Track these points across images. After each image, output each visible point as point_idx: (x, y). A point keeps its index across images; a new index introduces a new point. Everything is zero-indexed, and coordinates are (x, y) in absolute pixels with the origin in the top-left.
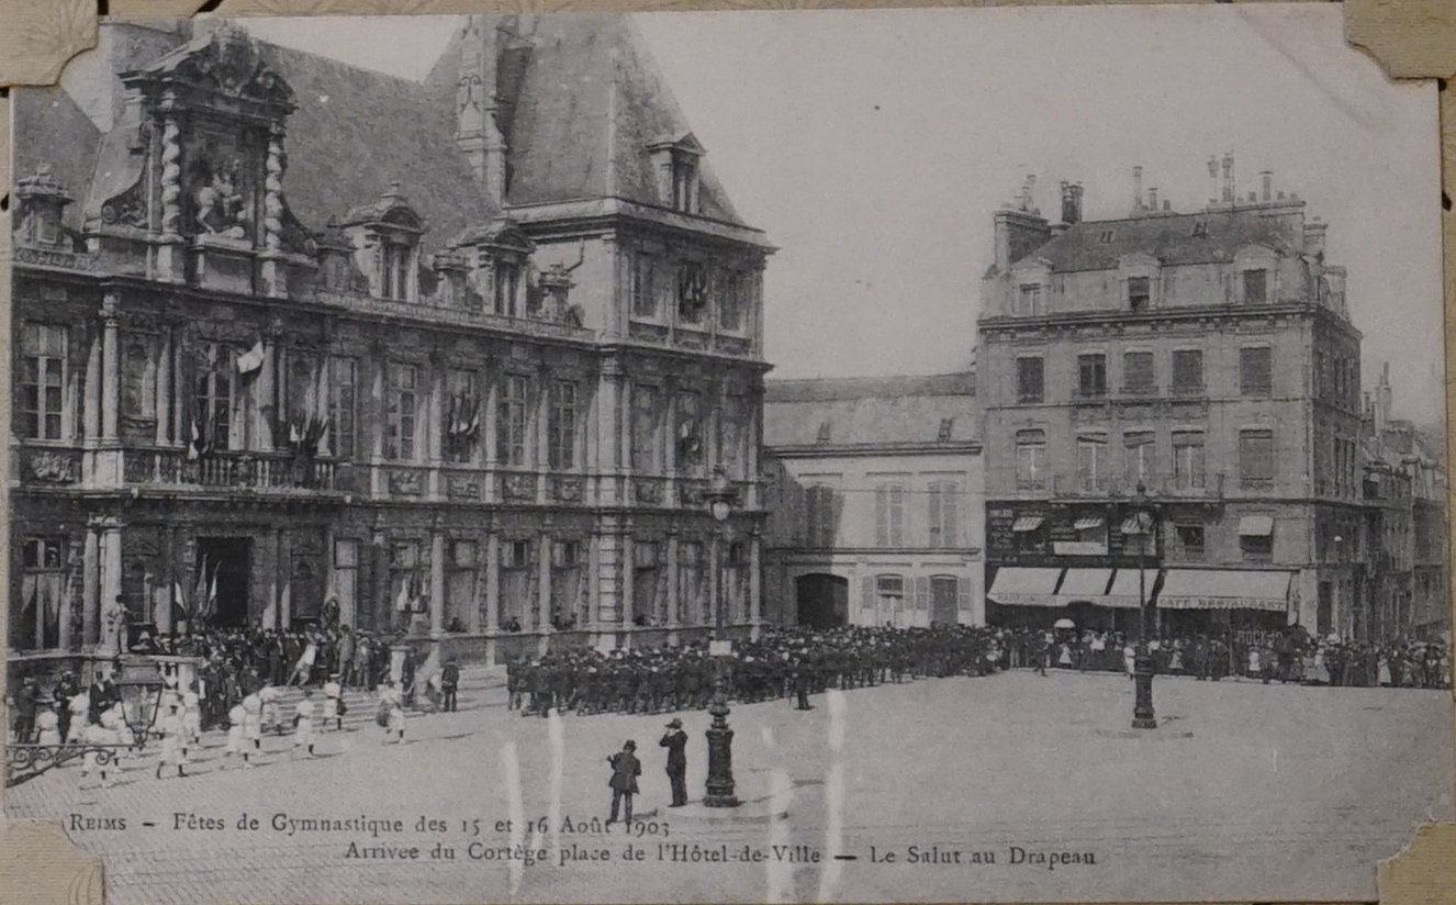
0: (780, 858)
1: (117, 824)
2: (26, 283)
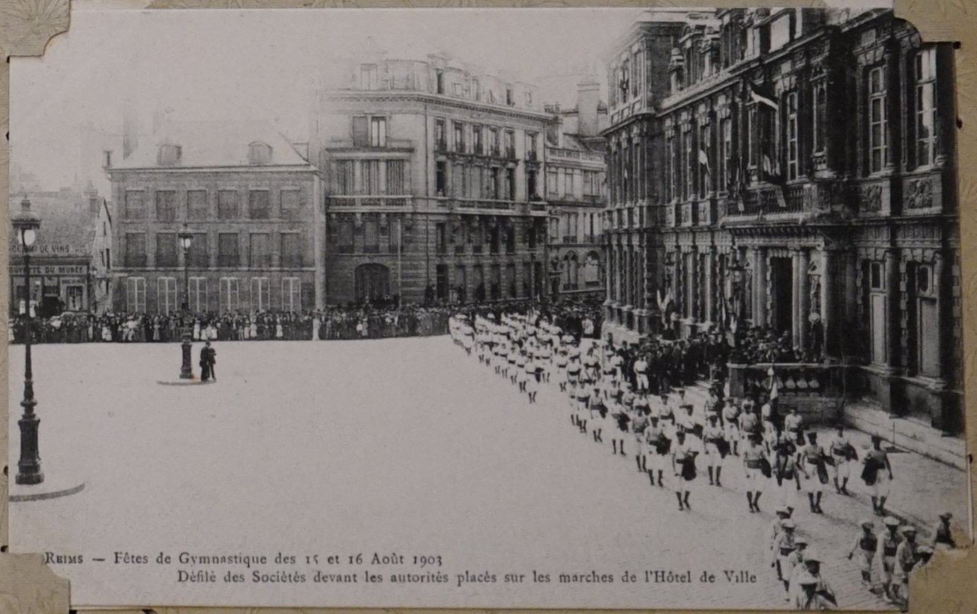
0: (730, 580)
2: (740, 13)
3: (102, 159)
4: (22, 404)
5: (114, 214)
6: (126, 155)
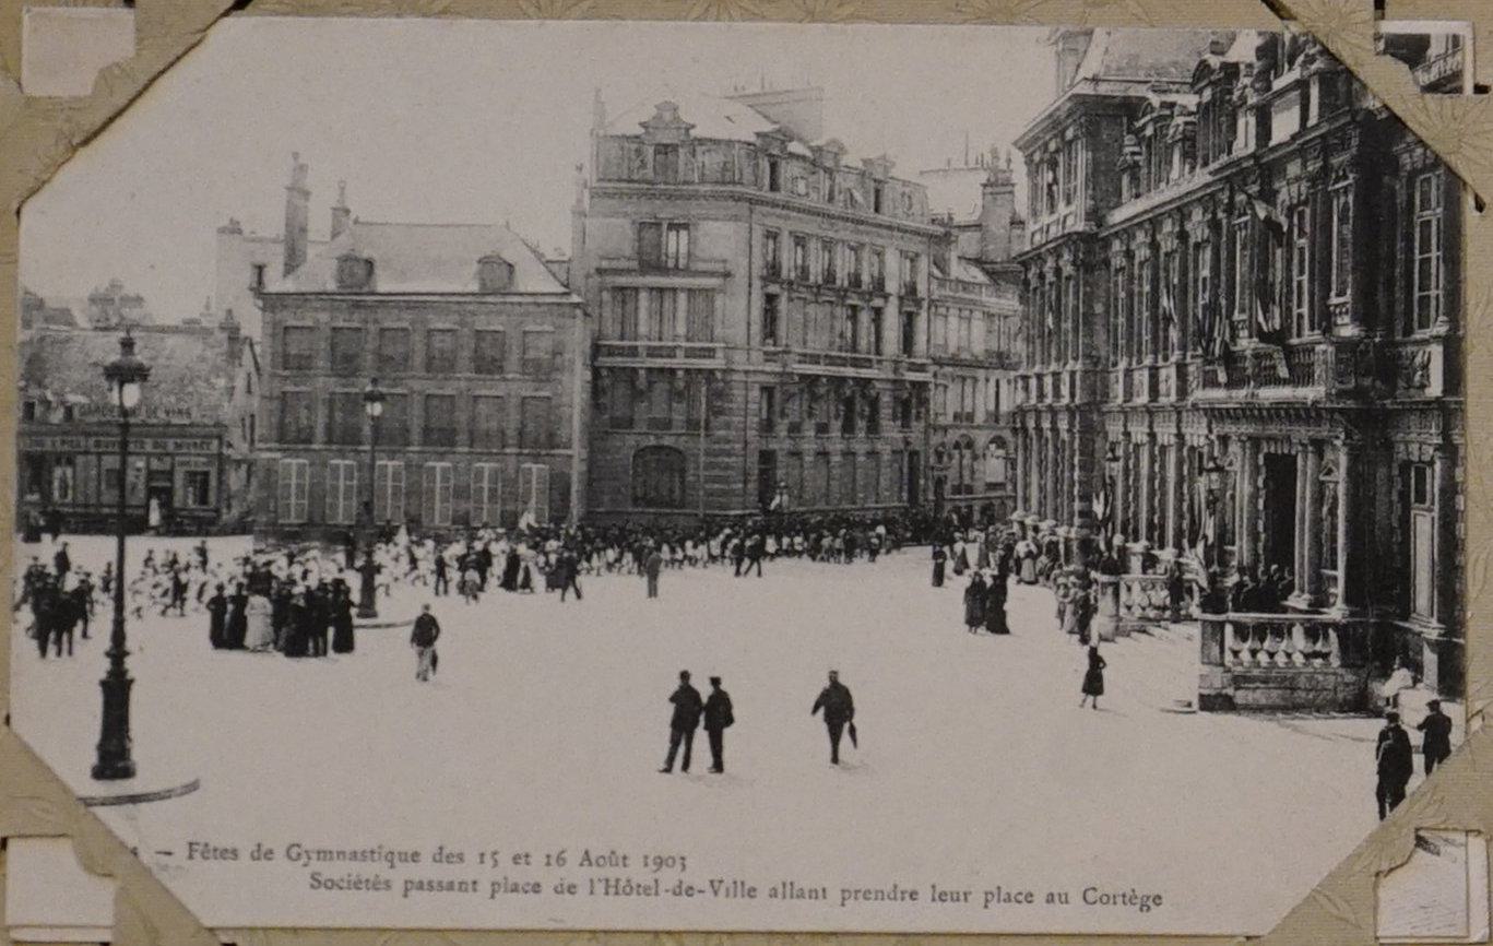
3: (248, 277)
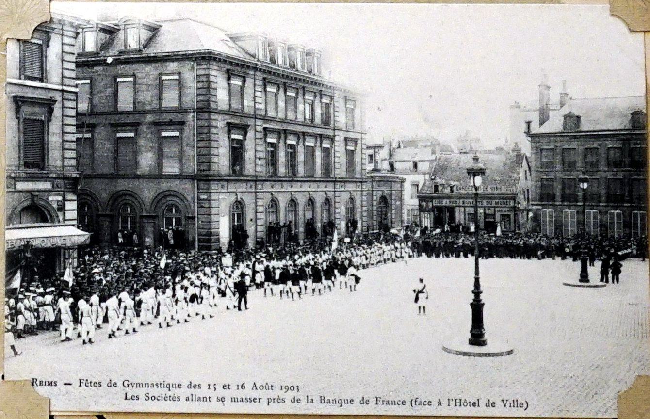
0: (505, 406)
1: (53, 383)
3: (524, 127)
4: (473, 292)
5: (533, 165)
6: (541, 124)
